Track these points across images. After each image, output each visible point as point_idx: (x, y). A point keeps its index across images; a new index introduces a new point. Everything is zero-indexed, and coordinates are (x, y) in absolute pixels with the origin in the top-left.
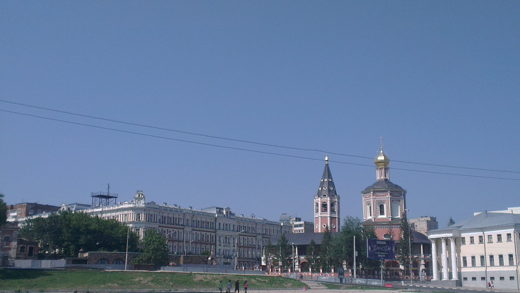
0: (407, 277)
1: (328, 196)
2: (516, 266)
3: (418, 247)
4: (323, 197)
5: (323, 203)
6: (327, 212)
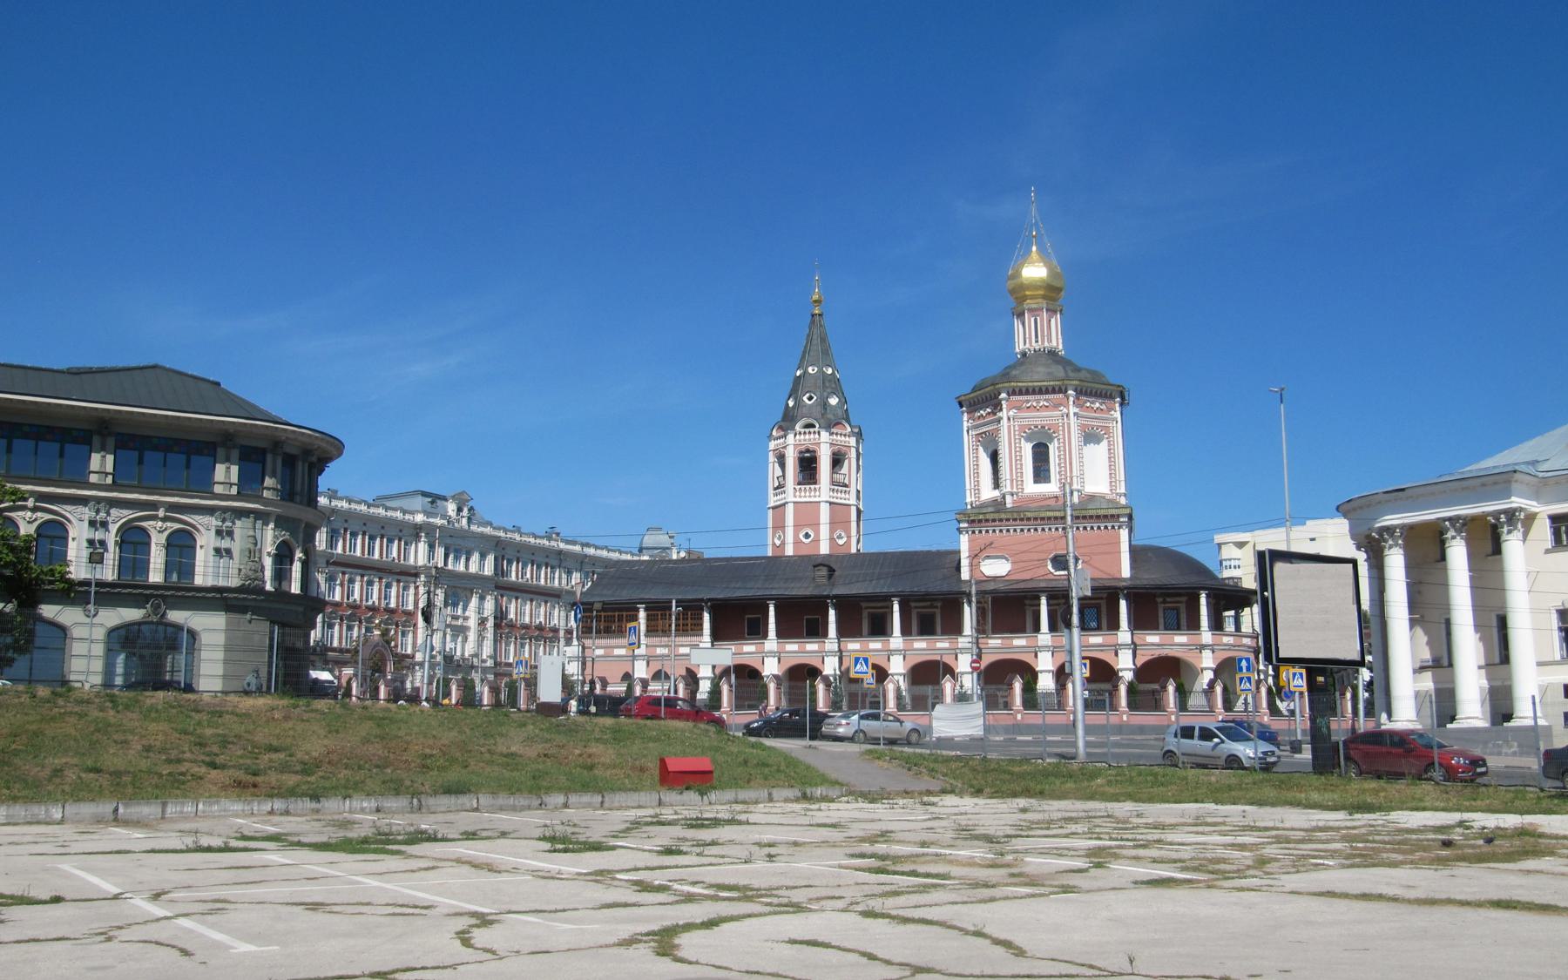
0: (808, 672)
1: (820, 427)
2: (89, 651)
3: (1058, 605)
4: (803, 430)
5: (801, 452)
6: (815, 483)
